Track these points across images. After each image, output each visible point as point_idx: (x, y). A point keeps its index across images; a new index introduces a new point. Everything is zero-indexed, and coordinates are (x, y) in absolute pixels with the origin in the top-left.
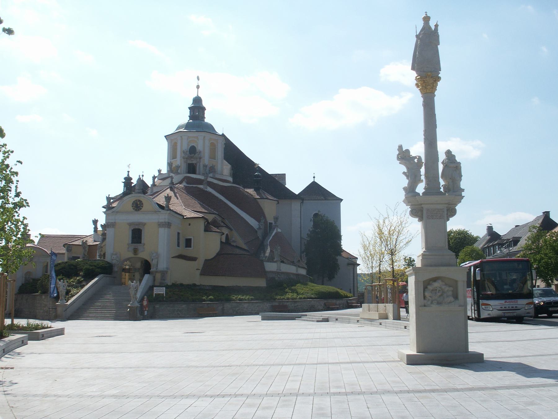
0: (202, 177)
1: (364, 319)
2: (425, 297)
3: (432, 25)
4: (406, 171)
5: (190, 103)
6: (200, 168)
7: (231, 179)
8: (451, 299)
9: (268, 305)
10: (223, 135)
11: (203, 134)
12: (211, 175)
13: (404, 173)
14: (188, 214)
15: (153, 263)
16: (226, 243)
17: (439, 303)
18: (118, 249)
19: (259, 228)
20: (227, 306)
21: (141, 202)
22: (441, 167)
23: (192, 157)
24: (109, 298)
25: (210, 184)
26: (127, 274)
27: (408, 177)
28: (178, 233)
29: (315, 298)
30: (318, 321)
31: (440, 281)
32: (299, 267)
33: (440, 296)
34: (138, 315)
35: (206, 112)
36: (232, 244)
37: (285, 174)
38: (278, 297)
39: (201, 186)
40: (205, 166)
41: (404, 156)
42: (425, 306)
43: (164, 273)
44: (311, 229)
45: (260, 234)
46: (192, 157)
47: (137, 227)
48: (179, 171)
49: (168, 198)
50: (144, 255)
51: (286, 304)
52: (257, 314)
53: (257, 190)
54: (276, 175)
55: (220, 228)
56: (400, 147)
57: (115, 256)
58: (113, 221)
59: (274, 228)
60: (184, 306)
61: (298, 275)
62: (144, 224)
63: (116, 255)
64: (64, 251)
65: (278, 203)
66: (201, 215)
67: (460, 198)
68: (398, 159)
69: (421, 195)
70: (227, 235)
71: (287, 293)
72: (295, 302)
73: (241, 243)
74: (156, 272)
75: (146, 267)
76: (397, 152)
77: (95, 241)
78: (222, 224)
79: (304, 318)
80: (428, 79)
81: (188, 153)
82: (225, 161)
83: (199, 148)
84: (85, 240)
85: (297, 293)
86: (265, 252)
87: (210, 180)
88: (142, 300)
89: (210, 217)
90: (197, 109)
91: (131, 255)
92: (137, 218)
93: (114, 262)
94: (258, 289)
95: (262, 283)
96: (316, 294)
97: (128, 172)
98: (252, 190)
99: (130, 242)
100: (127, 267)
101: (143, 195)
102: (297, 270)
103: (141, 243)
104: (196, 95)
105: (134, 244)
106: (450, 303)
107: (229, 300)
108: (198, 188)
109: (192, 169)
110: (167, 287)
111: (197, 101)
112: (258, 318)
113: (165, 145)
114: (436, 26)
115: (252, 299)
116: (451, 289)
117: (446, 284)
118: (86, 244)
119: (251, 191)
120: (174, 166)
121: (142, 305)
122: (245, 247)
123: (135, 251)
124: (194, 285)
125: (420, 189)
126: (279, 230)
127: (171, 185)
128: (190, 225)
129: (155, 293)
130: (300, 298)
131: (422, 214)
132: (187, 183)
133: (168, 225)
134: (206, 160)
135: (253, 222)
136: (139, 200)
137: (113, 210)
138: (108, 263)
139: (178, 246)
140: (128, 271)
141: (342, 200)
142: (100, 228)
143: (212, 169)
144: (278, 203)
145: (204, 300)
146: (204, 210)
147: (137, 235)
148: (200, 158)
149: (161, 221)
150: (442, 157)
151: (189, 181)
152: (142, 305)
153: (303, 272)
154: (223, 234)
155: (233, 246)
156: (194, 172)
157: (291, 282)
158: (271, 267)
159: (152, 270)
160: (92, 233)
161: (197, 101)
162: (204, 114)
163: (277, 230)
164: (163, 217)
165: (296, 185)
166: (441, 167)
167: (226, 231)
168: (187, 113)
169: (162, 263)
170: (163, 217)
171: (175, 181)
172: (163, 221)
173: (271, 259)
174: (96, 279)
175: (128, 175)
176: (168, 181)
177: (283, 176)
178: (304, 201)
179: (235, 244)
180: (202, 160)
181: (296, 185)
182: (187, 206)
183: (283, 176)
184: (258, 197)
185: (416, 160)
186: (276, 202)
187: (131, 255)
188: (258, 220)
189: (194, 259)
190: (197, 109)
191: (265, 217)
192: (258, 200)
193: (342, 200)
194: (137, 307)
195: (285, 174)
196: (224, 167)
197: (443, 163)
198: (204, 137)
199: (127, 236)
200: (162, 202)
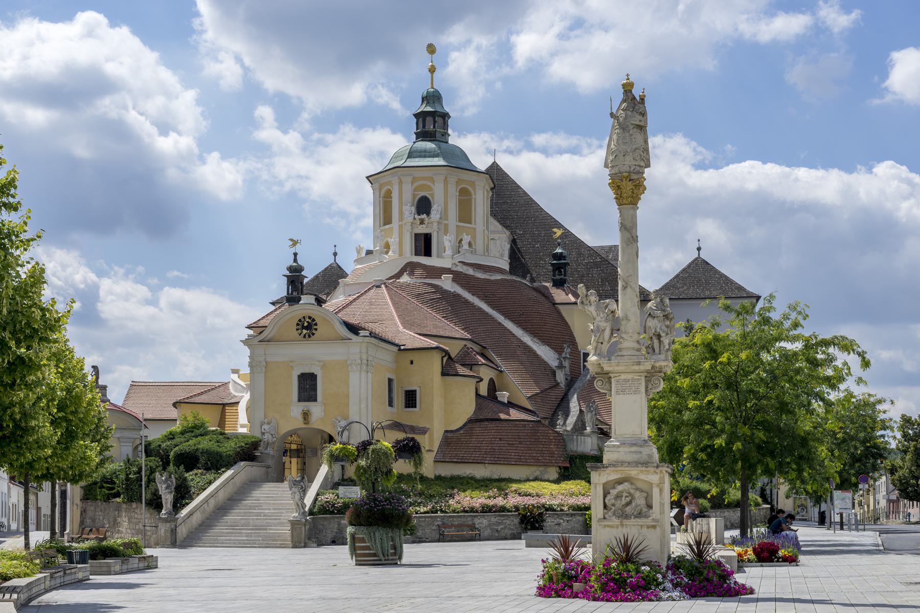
2: (605, 507)
3: (637, 93)
19: (561, 367)
26: (294, 460)
31: (626, 484)
33: (628, 504)
55: (474, 368)
57: (266, 427)
63: (269, 423)
70: (492, 382)
97: (295, 254)
98: (885, 168)
100: (294, 447)
128: (412, 362)
139: (391, 404)
147: (308, 386)
154: (481, 380)
156: (428, 253)
167: (486, 374)
174: (230, 473)
175: (295, 260)
188: (558, 350)
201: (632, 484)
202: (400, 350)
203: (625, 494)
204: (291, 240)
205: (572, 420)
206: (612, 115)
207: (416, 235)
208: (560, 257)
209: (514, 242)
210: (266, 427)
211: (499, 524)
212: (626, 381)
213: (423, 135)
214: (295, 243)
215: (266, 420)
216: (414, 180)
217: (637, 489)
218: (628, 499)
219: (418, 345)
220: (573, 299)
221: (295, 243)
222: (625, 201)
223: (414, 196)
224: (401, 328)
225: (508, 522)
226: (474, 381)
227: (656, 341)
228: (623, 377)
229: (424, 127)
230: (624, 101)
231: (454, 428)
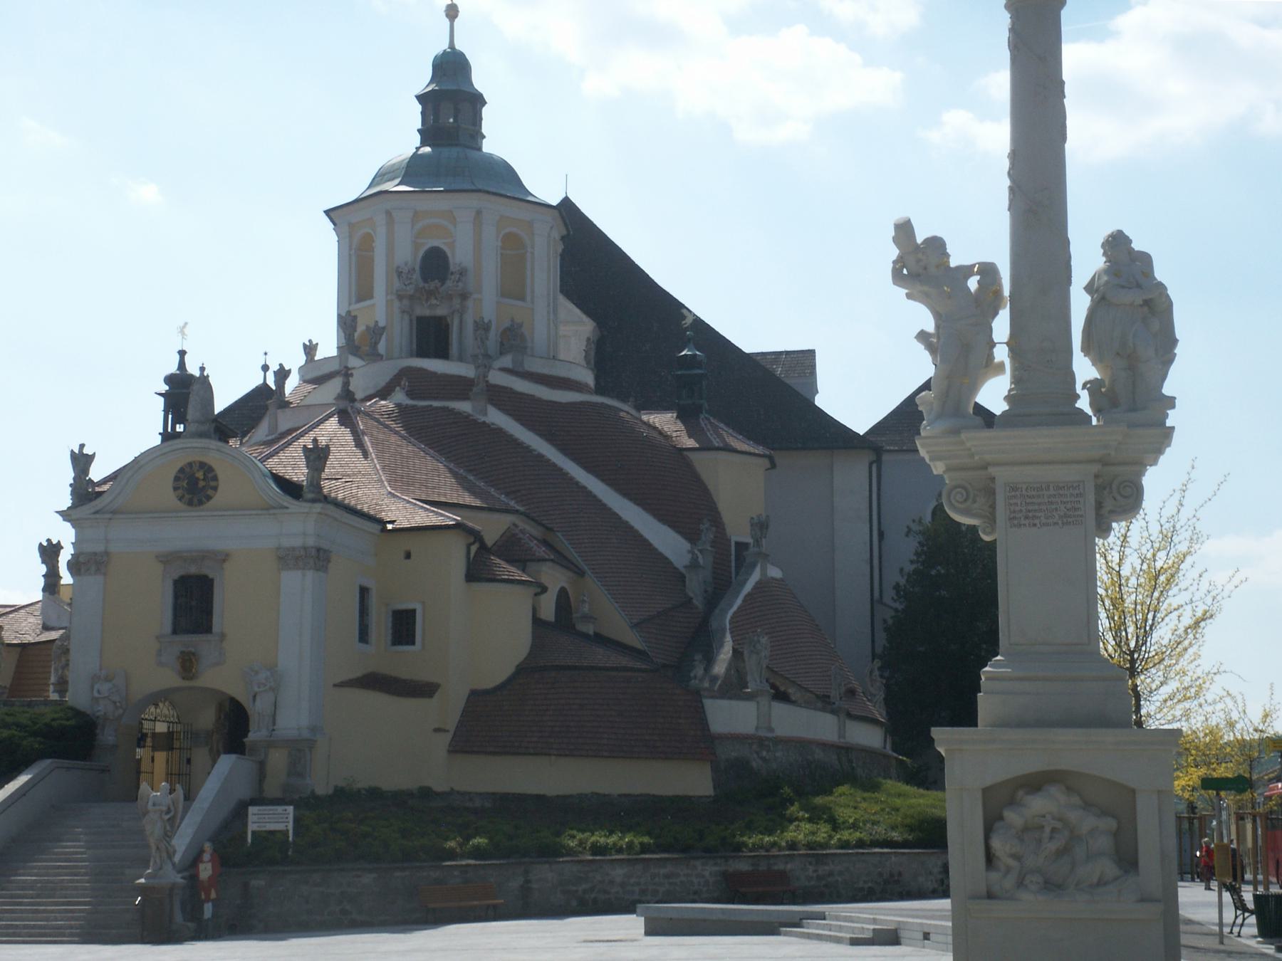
2: (990, 858)
4: (929, 325)
5: (422, 79)
6: (462, 335)
7: (588, 378)
8: (1108, 868)
9: (708, 870)
10: (567, 209)
11: (473, 201)
12: (507, 361)
13: (923, 336)
14: (404, 513)
15: (257, 709)
16: (559, 626)
17: (1051, 886)
18: (126, 663)
19: (694, 565)
20: (545, 874)
21: (211, 469)
22: (1080, 304)
23: (430, 294)
24: (73, 852)
25: (501, 398)
26: (161, 757)
27: (931, 348)
28: (364, 591)
29: (905, 844)
30: (855, 942)
31: (1055, 791)
32: (850, 716)
33: (1061, 853)
34: (178, 917)
35: (485, 111)
36: (581, 627)
37: (810, 354)
38: (751, 840)
39: (464, 407)
40: (482, 327)
41: (921, 265)
42: (990, 896)
43: (300, 749)
44: (910, 568)
45: (695, 587)
47: (193, 570)
48: (381, 348)
49: (318, 456)
50: (221, 677)
51: (780, 866)
52: (628, 908)
53: (687, 416)
56: (904, 231)
57: (105, 687)
58: (100, 548)
59: (754, 566)
60: (368, 879)
61: (845, 750)
62: (222, 558)
66: (449, 518)
67: (1158, 437)
68: (898, 277)
70: (563, 593)
71: (791, 821)
72: (820, 860)
73: (618, 625)
74: (271, 744)
75: (234, 727)
76: (894, 252)
77: (46, 628)
78: (541, 551)
79: (812, 928)
81: (417, 276)
82: (562, 299)
83: (461, 255)
85: (835, 826)
86: (709, 660)
87: (497, 378)
88: (194, 861)
89: (493, 527)
90: (451, 102)
91: (169, 678)
93: (101, 709)
94: (680, 807)
95: (694, 781)
96: (911, 828)
97: (182, 353)
99: (168, 628)
100: (161, 728)
101: (215, 444)
102: (842, 734)
103: (208, 629)
104: (444, 46)
105: (178, 638)
106: (1101, 883)
107: (551, 852)
108: (451, 411)
109: (432, 337)
110: (307, 804)
111: (451, 68)
112: (632, 924)
113: (325, 248)
115: (645, 849)
116: (1111, 824)
117: (1087, 805)
119: (664, 421)
120: (361, 328)
121: (193, 878)
122: (632, 638)
123: (188, 664)
124: (426, 793)
126: (774, 572)
127: (343, 404)
128: (408, 556)
129: (252, 827)
130: (844, 845)
131: (993, 507)
132: (410, 394)
133: (318, 558)
134: (487, 302)
135: (667, 542)
136: (202, 465)
137: (99, 503)
138: (77, 713)
139: (364, 636)
140: (166, 742)
142: (66, 578)
143: (513, 339)
145: (452, 855)
146: (468, 499)
147: (194, 600)
148: (464, 296)
149: (287, 543)
150: (1087, 261)
151: (417, 383)
152: (193, 878)
153: (869, 737)
154: (544, 589)
155: (585, 636)
156: (442, 353)
157: (816, 776)
158: (730, 717)
159: (252, 736)
160: (38, 596)
161: (451, 68)
163: (764, 570)
164: (299, 526)
166: (1080, 304)
167: (554, 578)
168: (413, 116)
169: (292, 711)
170: (299, 526)
171: (360, 385)
172: (297, 542)
173: (734, 687)
174: (23, 779)
175: (182, 365)
176: (332, 390)
177: (804, 361)
178: (885, 457)
182: (401, 481)
183: (804, 361)
184: (691, 443)
185: (973, 283)
186: (766, 462)
187: (169, 678)
188: (691, 536)
189: (423, 690)
190: (451, 102)
191: (717, 521)
192: (692, 456)
194: (173, 887)
195: (810, 354)
196: (563, 330)
197: (1089, 288)
198: (479, 213)
199: (158, 604)
200: (298, 472)
202: (384, 530)
207: (421, 320)
229: (436, 119)
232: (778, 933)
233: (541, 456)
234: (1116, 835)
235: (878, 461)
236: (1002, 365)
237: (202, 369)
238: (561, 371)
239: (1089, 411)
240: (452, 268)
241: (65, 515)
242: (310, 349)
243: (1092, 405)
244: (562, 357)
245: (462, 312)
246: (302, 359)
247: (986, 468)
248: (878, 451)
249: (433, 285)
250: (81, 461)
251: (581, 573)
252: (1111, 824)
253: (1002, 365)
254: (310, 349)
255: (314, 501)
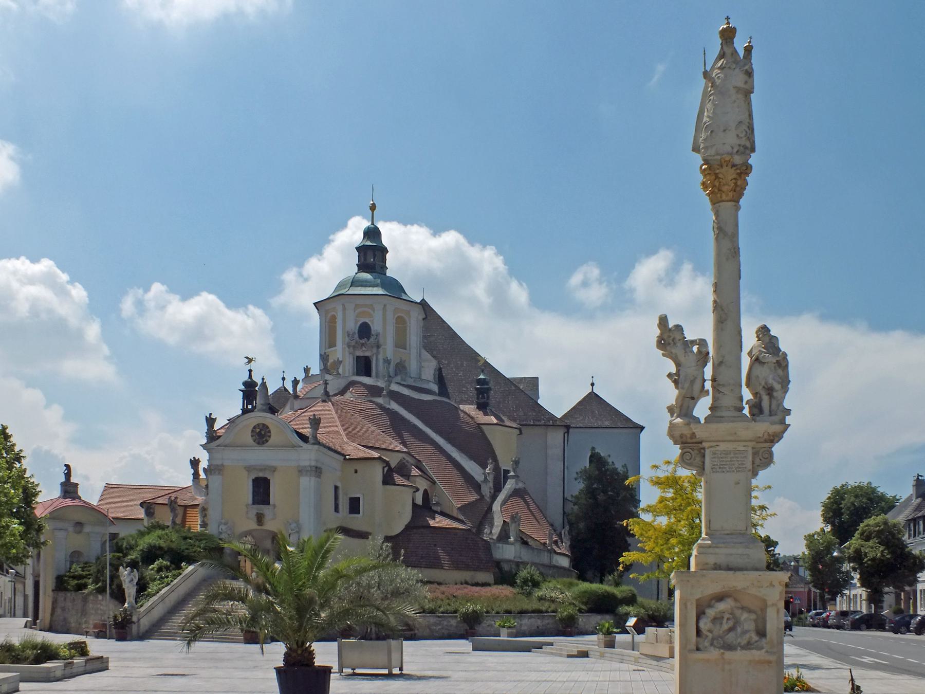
0: (381, 384)
1: (646, 655)
2: (699, 632)
7: (435, 388)
12: (398, 379)
18: (230, 517)
23: (363, 345)
25: (394, 396)
28: (336, 488)
33: (731, 630)
35: (388, 256)
36: (434, 508)
37: (537, 378)
40: (387, 361)
41: (670, 338)
46: (363, 345)
47: (261, 475)
49: (315, 422)
50: (271, 525)
54: (522, 380)
57: (223, 527)
62: (274, 469)
63: (225, 524)
64: (141, 513)
65: (521, 433)
69: (703, 421)
70: (426, 491)
80: (725, 168)
81: (356, 336)
82: (424, 353)
83: (376, 327)
84: (173, 496)
87: (394, 387)
92: (260, 456)
97: (250, 371)
101: (270, 415)
103: (268, 503)
105: (255, 506)
109: (364, 366)
114: (748, 50)
116: (753, 616)
118: (176, 503)
120: (331, 361)
123: (260, 519)
125: (702, 409)
128: (356, 472)
133: (317, 471)
134: (389, 349)
139: (336, 509)
141: (642, 428)
142: (202, 475)
143: (401, 368)
144: (521, 433)
147: (261, 490)
148: (378, 347)
154: (418, 490)
156: (368, 373)
162: (384, 260)
164: (308, 455)
165: (558, 400)
172: (307, 463)
175: (250, 376)
177: (534, 382)
178: (571, 430)
179: (438, 509)
180: (381, 350)
181: (558, 400)
186: (518, 432)
187: (252, 525)
191: (495, 460)
193: (642, 428)
195: (537, 378)
197: (750, 354)
199: (246, 492)
200: (307, 431)
201: (736, 600)
202: (345, 459)
203: (726, 616)
204: (247, 358)
205: (496, 530)
206: (706, 74)
207: (358, 357)
208: (480, 382)
209: (440, 370)
210: (223, 527)
211: (439, 624)
212: (727, 453)
213: (362, 267)
214: (250, 360)
215: (223, 521)
216: (357, 306)
217: (743, 608)
218: (731, 623)
219: (360, 455)
220: (495, 421)
221: (250, 360)
222: (724, 197)
223: (356, 322)
224: (345, 439)
225: (445, 623)
226: (412, 490)
227: (765, 398)
228: (723, 446)
229: (365, 259)
230: (722, 56)
231: (393, 534)
232: (530, 651)
233: (415, 425)
234: (756, 621)
235: (568, 432)
236: (708, 391)
237: (263, 379)
238: (425, 386)
239: (748, 415)
240: (373, 332)
241: (204, 446)
242: (307, 370)
243: (750, 412)
244: (423, 377)
245: (377, 354)
246: (303, 375)
247: (701, 443)
248: (568, 427)
249: (363, 341)
250: (210, 421)
251: (434, 483)
252: (753, 616)
253: (708, 391)
254: (307, 370)
255: (314, 444)
